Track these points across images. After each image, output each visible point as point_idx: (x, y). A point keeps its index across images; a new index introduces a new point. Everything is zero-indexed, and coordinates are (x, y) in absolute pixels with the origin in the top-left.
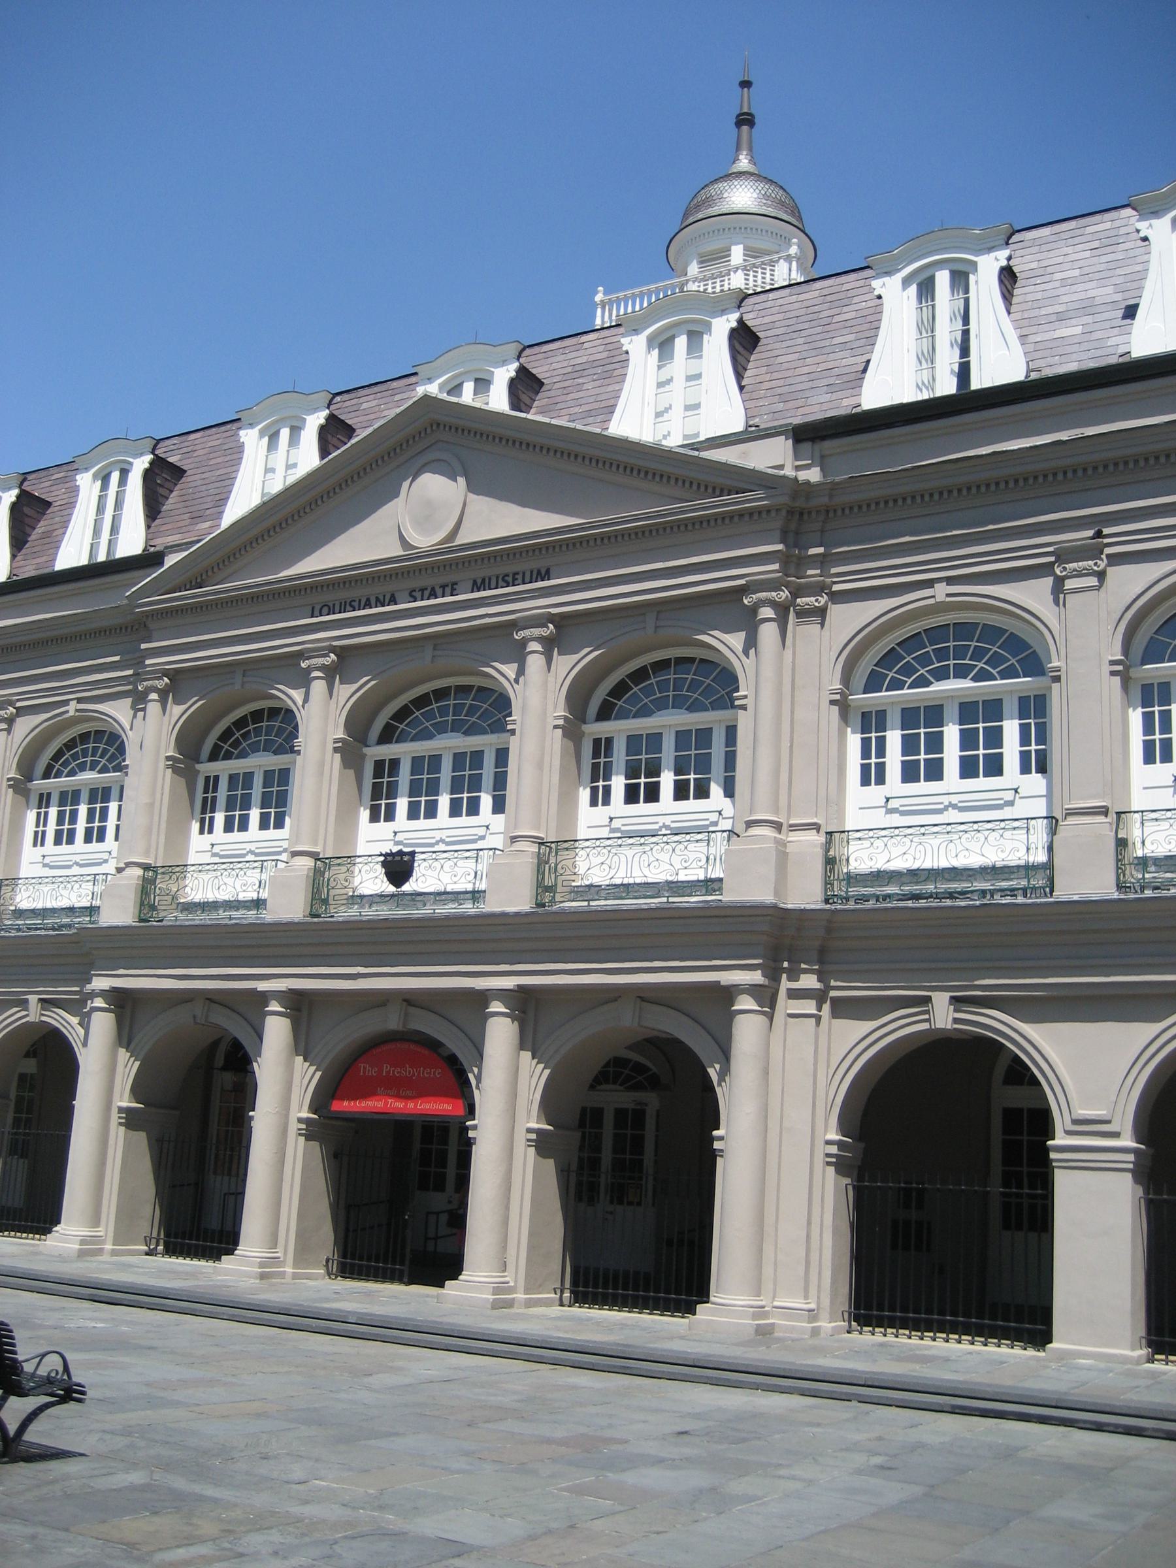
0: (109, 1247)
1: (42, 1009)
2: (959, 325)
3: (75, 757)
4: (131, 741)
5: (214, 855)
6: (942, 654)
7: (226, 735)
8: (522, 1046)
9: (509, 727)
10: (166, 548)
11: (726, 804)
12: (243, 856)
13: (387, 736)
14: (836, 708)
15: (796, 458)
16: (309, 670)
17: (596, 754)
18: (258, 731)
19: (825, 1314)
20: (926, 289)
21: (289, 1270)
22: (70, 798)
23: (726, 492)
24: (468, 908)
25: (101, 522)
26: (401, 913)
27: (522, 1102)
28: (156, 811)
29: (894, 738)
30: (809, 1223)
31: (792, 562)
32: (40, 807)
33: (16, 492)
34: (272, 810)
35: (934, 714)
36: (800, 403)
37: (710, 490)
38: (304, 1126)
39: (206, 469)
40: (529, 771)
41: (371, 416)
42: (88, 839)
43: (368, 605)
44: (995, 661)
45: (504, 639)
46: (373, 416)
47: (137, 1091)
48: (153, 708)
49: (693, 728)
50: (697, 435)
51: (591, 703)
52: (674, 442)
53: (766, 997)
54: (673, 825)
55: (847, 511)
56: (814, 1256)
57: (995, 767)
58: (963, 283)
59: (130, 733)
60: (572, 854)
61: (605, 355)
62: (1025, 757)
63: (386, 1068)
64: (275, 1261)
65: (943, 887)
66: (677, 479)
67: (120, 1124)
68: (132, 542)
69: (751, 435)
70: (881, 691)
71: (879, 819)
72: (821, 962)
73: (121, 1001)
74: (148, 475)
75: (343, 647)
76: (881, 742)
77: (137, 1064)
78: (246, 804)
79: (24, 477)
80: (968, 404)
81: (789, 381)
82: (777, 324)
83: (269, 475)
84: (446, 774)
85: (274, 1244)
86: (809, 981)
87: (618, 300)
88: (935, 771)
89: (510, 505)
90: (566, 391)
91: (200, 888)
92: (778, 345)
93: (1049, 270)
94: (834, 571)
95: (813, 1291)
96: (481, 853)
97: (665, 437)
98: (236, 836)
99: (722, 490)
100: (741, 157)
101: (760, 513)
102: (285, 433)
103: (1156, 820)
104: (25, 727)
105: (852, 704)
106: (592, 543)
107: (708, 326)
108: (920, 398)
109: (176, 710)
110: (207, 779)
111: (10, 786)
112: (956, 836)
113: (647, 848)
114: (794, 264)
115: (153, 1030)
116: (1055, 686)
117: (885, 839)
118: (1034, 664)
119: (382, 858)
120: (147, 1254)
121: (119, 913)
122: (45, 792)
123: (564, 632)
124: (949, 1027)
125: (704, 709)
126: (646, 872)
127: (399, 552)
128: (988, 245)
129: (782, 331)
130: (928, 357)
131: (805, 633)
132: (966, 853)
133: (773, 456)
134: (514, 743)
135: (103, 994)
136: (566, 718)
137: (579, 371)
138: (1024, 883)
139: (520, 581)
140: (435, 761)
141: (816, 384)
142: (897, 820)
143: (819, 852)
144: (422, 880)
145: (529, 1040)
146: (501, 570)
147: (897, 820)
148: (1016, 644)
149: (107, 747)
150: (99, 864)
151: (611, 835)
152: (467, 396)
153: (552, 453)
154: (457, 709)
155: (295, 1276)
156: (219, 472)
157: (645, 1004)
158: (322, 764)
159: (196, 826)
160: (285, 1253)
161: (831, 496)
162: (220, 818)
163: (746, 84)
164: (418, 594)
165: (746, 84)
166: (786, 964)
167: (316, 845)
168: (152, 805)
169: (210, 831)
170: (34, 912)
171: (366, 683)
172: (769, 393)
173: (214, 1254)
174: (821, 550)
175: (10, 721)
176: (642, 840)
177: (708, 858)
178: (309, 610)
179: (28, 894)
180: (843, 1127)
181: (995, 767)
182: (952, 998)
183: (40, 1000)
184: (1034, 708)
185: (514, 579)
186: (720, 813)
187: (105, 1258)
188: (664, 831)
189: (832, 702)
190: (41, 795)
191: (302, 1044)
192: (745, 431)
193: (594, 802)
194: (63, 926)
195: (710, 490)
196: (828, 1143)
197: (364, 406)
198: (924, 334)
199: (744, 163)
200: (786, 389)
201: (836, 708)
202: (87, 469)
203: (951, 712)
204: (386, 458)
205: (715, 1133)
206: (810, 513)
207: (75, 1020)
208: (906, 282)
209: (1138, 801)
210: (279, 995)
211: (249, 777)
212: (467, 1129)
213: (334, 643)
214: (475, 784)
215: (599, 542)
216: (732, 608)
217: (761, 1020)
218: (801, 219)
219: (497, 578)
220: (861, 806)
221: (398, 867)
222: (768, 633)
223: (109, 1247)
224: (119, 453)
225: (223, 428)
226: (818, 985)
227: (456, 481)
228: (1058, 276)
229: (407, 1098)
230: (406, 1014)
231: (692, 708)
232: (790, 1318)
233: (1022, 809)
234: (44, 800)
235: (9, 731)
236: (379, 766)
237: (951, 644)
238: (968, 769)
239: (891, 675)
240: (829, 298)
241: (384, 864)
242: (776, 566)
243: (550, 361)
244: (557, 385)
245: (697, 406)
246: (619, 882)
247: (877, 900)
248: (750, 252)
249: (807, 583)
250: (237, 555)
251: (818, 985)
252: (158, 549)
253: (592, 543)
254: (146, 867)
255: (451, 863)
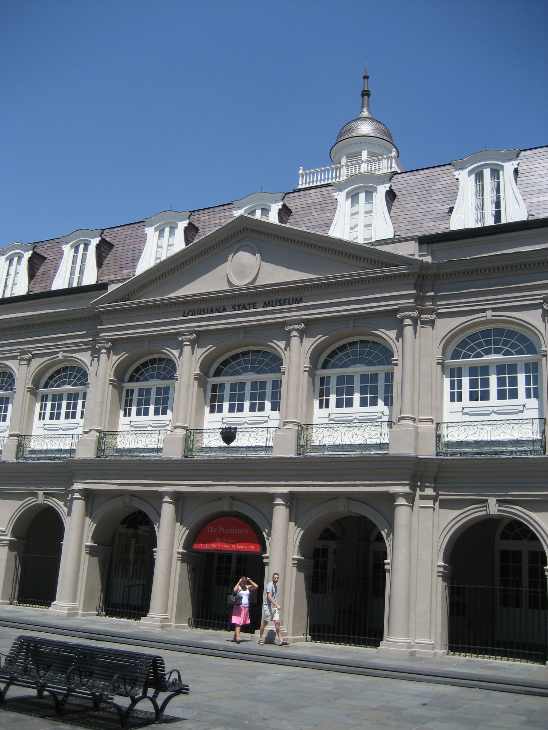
0: (81, 612)
1: (45, 497)
2: (495, 194)
3: (60, 378)
4: (91, 371)
5: (131, 426)
6: (488, 343)
7: (137, 370)
8: (290, 520)
9: (282, 371)
10: (109, 281)
11: (386, 410)
12: (146, 427)
13: (218, 373)
14: (440, 366)
15: (420, 251)
16: (182, 341)
17: (322, 384)
18: (153, 369)
19: (438, 646)
20: (479, 177)
21: (173, 624)
22: (57, 397)
23: (388, 266)
24: (263, 454)
25: (77, 267)
26: (228, 456)
27: (290, 546)
28: (105, 405)
29: (466, 381)
30: (431, 604)
31: (419, 299)
32: (42, 401)
33: (31, 252)
34: (161, 406)
35: (485, 370)
36: (419, 226)
37: (380, 264)
38: (180, 556)
39: (124, 245)
40: (183, 394)
41: (210, 225)
42: (67, 417)
43: (212, 311)
44: (513, 346)
45: (280, 330)
46: (207, 223)
47: (94, 538)
48: (104, 357)
49: (369, 373)
50: (371, 238)
51: (321, 360)
52: (360, 241)
53: (410, 498)
54: (360, 418)
55: (445, 276)
56: (433, 619)
57: (514, 395)
58: (496, 175)
59: (90, 368)
60: (201, 435)
61: (321, 200)
62: (528, 391)
63: (221, 529)
64: (166, 620)
65: (492, 449)
66: (364, 259)
67: (86, 553)
68: (90, 277)
69: (396, 240)
70: (459, 359)
71: (459, 417)
72: (435, 483)
73: (87, 495)
74: (98, 247)
75: (199, 331)
76: (460, 382)
77: (95, 525)
78: (148, 403)
79: (35, 246)
80: (500, 230)
81: (412, 216)
82: (404, 189)
83: (159, 249)
84: (248, 391)
85: (166, 612)
86: (429, 491)
87: (310, 174)
88: (485, 396)
89: (282, 268)
90: (303, 216)
91: (122, 443)
92: (405, 199)
93: (533, 170)
94: (438, 303)
95: (433, 635)
96: (269, 429)
97: (355, 239)
98: (142, 418)
99: (386, 265)
100: (364, 110)
101: (404, 276)
102: (167, 230)
103: (453, 426)
104: (36, 363)
105: (446, 365)
106: (323, 287)
107: (376, 190)
108: (477, 227)
109: (114, 358)
110: (128, 390)
111: (28, 391)
112: (498, 426)
113: (351, 429)
114: (394, 160)
115: (104, 508)
116: (544, 359)
117: (513, 425)
118: (532, 349)
119: (221, 430)
120: (97, 615)
121: (86, 453)
122: (45, 394)
123: (309, 327)
124: (496, 513)
125: (375, 365)
126: (351, 439)
127: (226, 287)
128: (509, 158)
129: (407, 192)
130: (481, 206)
131: (424, 331)
132: (504, 434)
133: (409, 250)
134: (284, 378)
135: (79, 491)
136: (310, 367)
137: (309, 207)
138: (532, 448)
139: (287, 303)
140: (242, 385)
141: (425, 217)
142: (467, 418)
143: (433, 432)
144: (240, 441)
145: (294, 517)
146: (278, 298)
147: (133, 429)
148: (523, 339)
149: (80, 375)
150: (73, 429)
151: (330, 422)
152: (258, 215)
153: (303, 245)
154: (253, 361)
155: (176, 627)
156: (131, 247)
157: (350, 501)
158: (188, 386)
159: (122, 413)
160: (171, 615)
161: (438, 269)
162: (134, 409)
163: (366, 77)
164: (237, 308)
165: (366, 77)
166: (419, 484)
167: (186, 423)
168: (102, 402)
169: (129, 415)
170: (40, 451)
171: (210, 348)
172: (404, 221)
173: (137, 617)
174: (433, 294)
175: (29, 360)
176: (349, 425)
177: (381, 434)
178: (182, 313)
179: (39, 443)
180: (445, 561)
181: (514, 395)
182: (497, 500)
183: (44, 493)
184: (532, 369)
185: (284, 302)
186: (382, 413)
187: (79, 617)
188: (355, 421)
189: (438, 363)
190: (43, 396)
191: (180, 517)
192: (394, 238)
193: (321, 407)
194: (56, 458)
195: (380, 264)
196: (439, 566)
197: (202, 218)
198: (478, 197)
199: (365, 113)
200: (411, 219)
201: (440, 366)
202: (67, 243)
203: (493, 369)
204: (221, 243)
205: (385, 561)
206: (427, 276)
207: (62, 503)
208: (470, 173)
209: (446, 418)
210: (169, 494)
211: (149, 390)
212: (263, 558)
213: (195, 329)
214: (262, 397)
215: (326, 286)
216: (392, 319)
217: (408, 509)
218: (392, 140)
219: (276, 301)
220: (450, 411)
221: (228, 435)
222: (408, 331)
223: (81, 612)
224: (84, 236)
225: (131, 226)
226: (434, 494)
227: (255, 256)
228: (537, 173)
229: (232, 543)
230: (232, 503)
231: (368, 364)
232: (424, 648)
233: (527, 414)
234: (44, 398)
235: (28, 365)
236: (214, 387)
237: (492, 338)
238: (501, 395)
239: (464, 351)
240: (428, 178)
241: (222, 433)
242: (412, 301)
243: (294, 201)
244: (298, 213)
245: (370, 225)
246: (338, 444)
247: (461, 455)
248: (370, 154)
249: (426, 309)
250: (147, 286)
251: (434, 494)
252: (103, 282)
253: (323, 287)
254: (100, 432)
255: (254, 433)
